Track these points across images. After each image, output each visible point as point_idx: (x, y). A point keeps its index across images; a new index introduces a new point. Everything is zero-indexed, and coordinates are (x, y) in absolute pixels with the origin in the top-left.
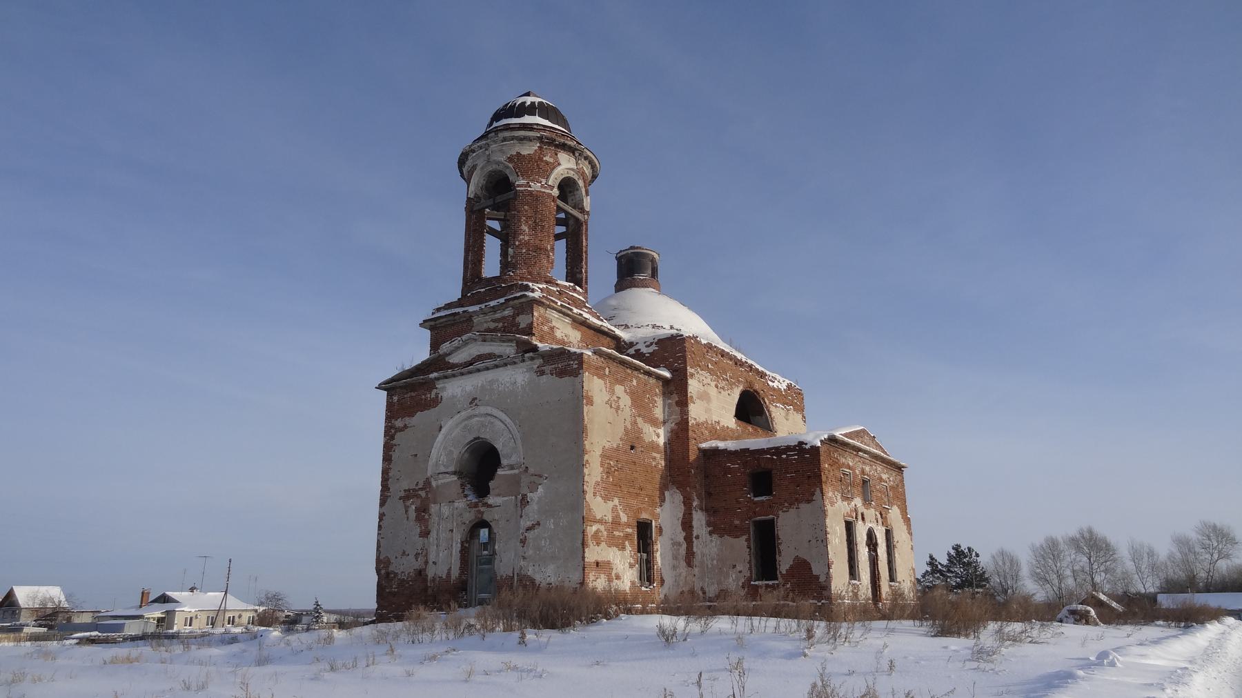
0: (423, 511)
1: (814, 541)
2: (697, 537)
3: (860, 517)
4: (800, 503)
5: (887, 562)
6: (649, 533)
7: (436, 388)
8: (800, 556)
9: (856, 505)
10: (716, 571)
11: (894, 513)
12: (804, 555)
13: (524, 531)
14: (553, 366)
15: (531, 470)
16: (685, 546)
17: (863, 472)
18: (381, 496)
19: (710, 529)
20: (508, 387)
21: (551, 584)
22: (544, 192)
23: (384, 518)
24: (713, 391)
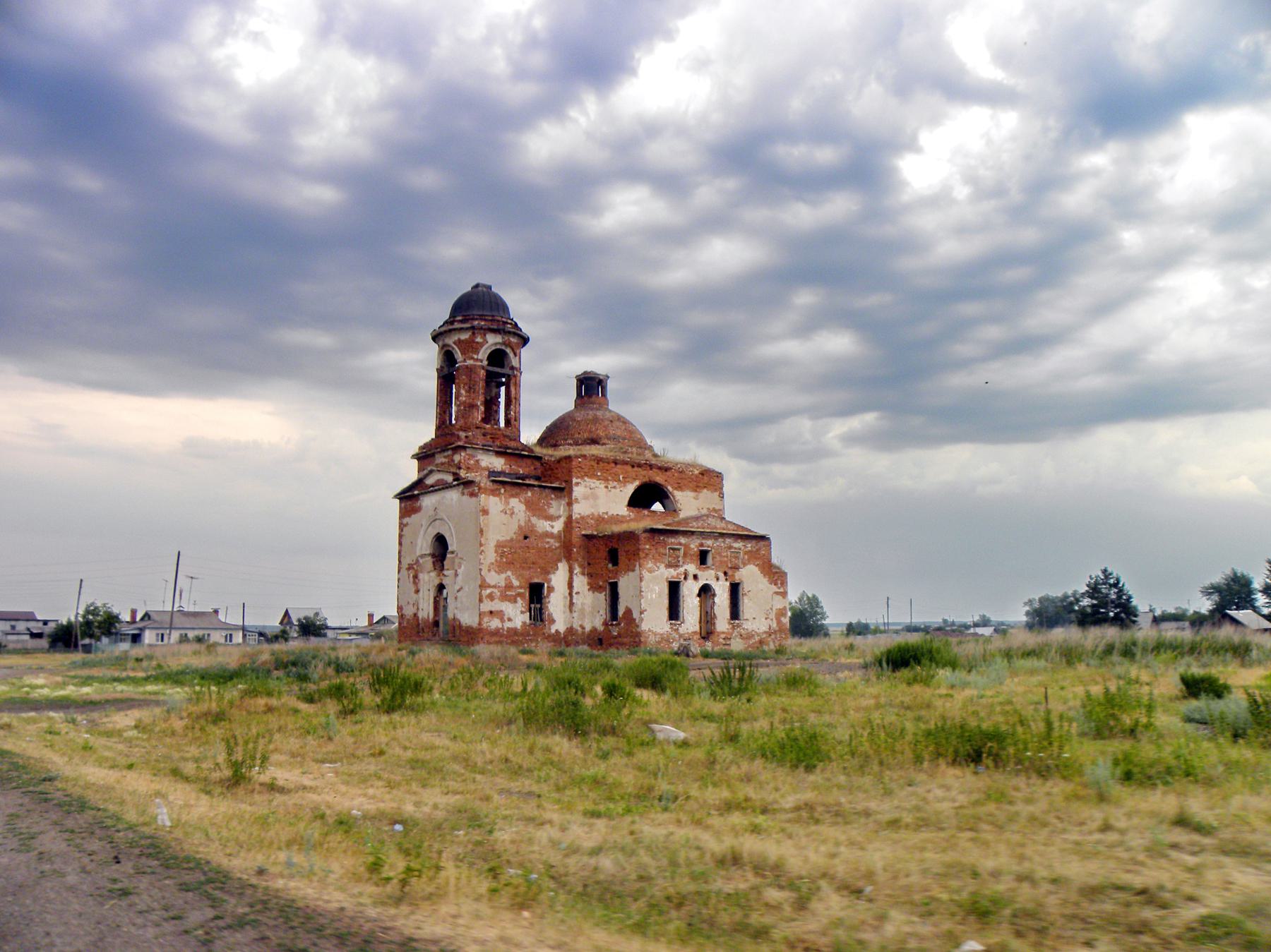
0: (416, 577)
2: (578, 593)
15: (459, 555)
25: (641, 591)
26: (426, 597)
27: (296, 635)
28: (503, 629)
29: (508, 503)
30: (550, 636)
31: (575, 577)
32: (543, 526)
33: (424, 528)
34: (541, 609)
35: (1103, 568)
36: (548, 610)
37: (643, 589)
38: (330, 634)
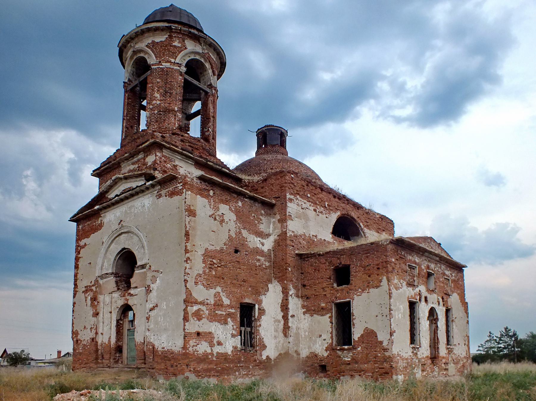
0: (94, 299)
1: (380, 316)
2: (293, 316)
3: (423, 299)
4: (370, 288)
5: (445, 331)
6: (253, 314)
7: (101, 217)
8: (369, 327)
9: (420, 291)
10: (308, 339)
11: (454, 299)
12: (371, 327)
13: (149, 311)
14: (167, 190)
15: (153, 268)
16: (282, 322)
17: (428, 267)
18: (74, 291)
19: (305, 310)
20: (140, 210)
21: (164, 348)
22: (173, 69)
23: (75, 305)
24: (311, 213)
25: (390, 310)
26: (107, 322)
27: (6, 363)
28: (212, 354)
29: (218, 209)
30: (261, 362)
31: (290, 298)
32: (254, 241)
33: (105, 246)
34: (251, 333)
35: (505, 327)
36: (259, 334)
37: (392, 307)
38: (33, 363)
